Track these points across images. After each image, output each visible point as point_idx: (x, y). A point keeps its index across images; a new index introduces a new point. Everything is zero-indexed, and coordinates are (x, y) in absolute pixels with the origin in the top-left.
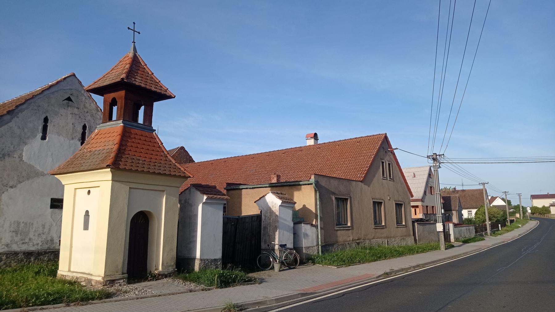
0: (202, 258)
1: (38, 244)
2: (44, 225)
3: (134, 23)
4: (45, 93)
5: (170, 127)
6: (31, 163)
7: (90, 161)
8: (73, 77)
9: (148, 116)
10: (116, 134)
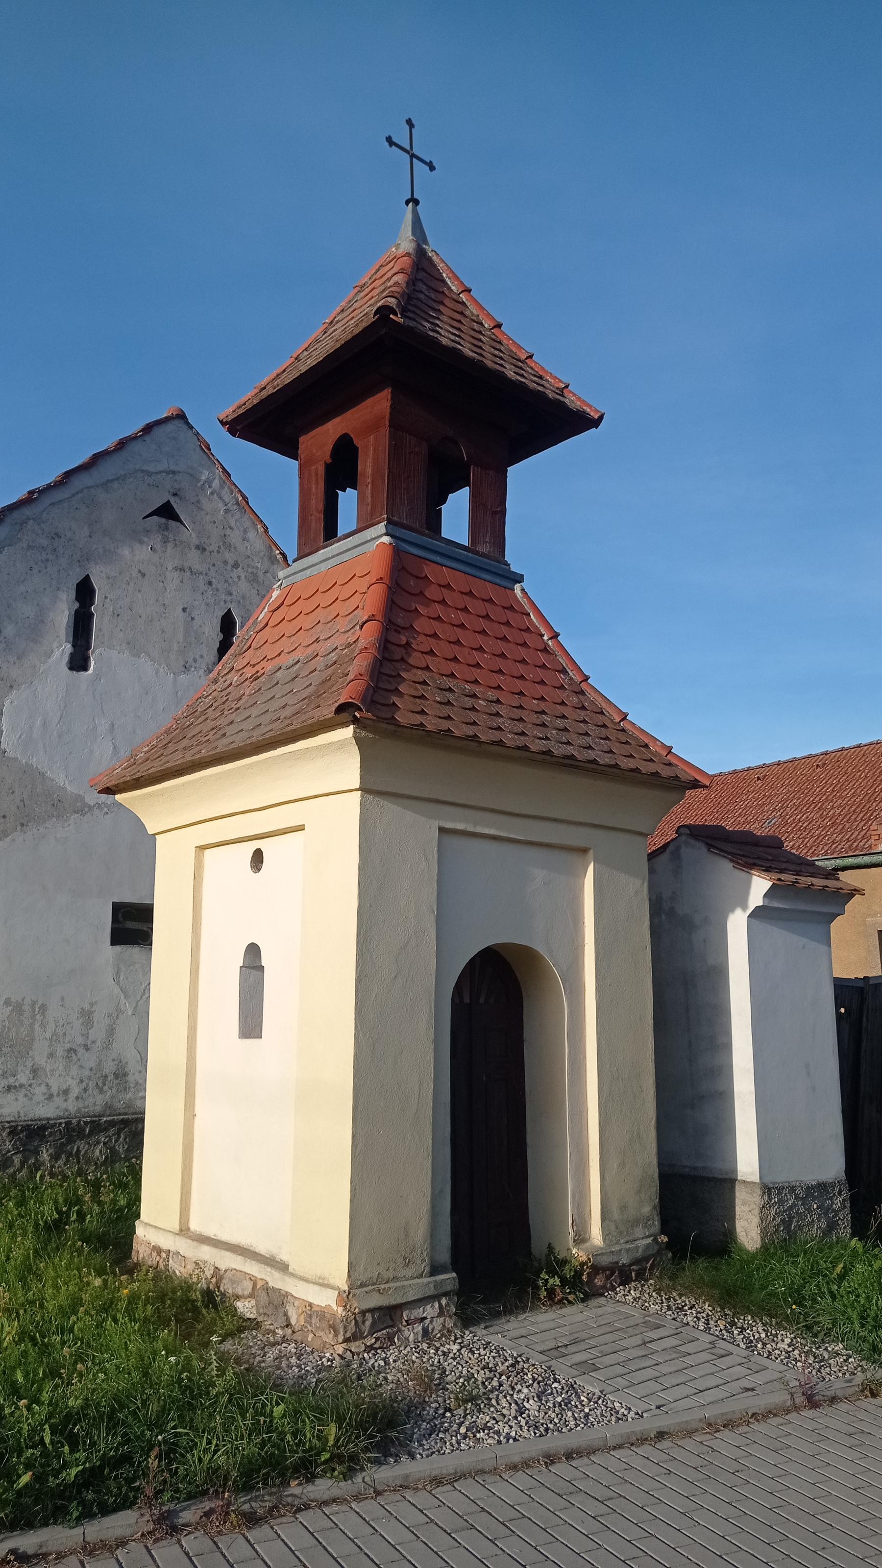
0: (768, 1180)
1: (66, 1092)
2: (90, 1013)
3: (409, 122)
4: (78, 483)
6: (34, 761)
7: (254, 712)
8: (179, 423)
9: (490, 516)
10: (361, 585)
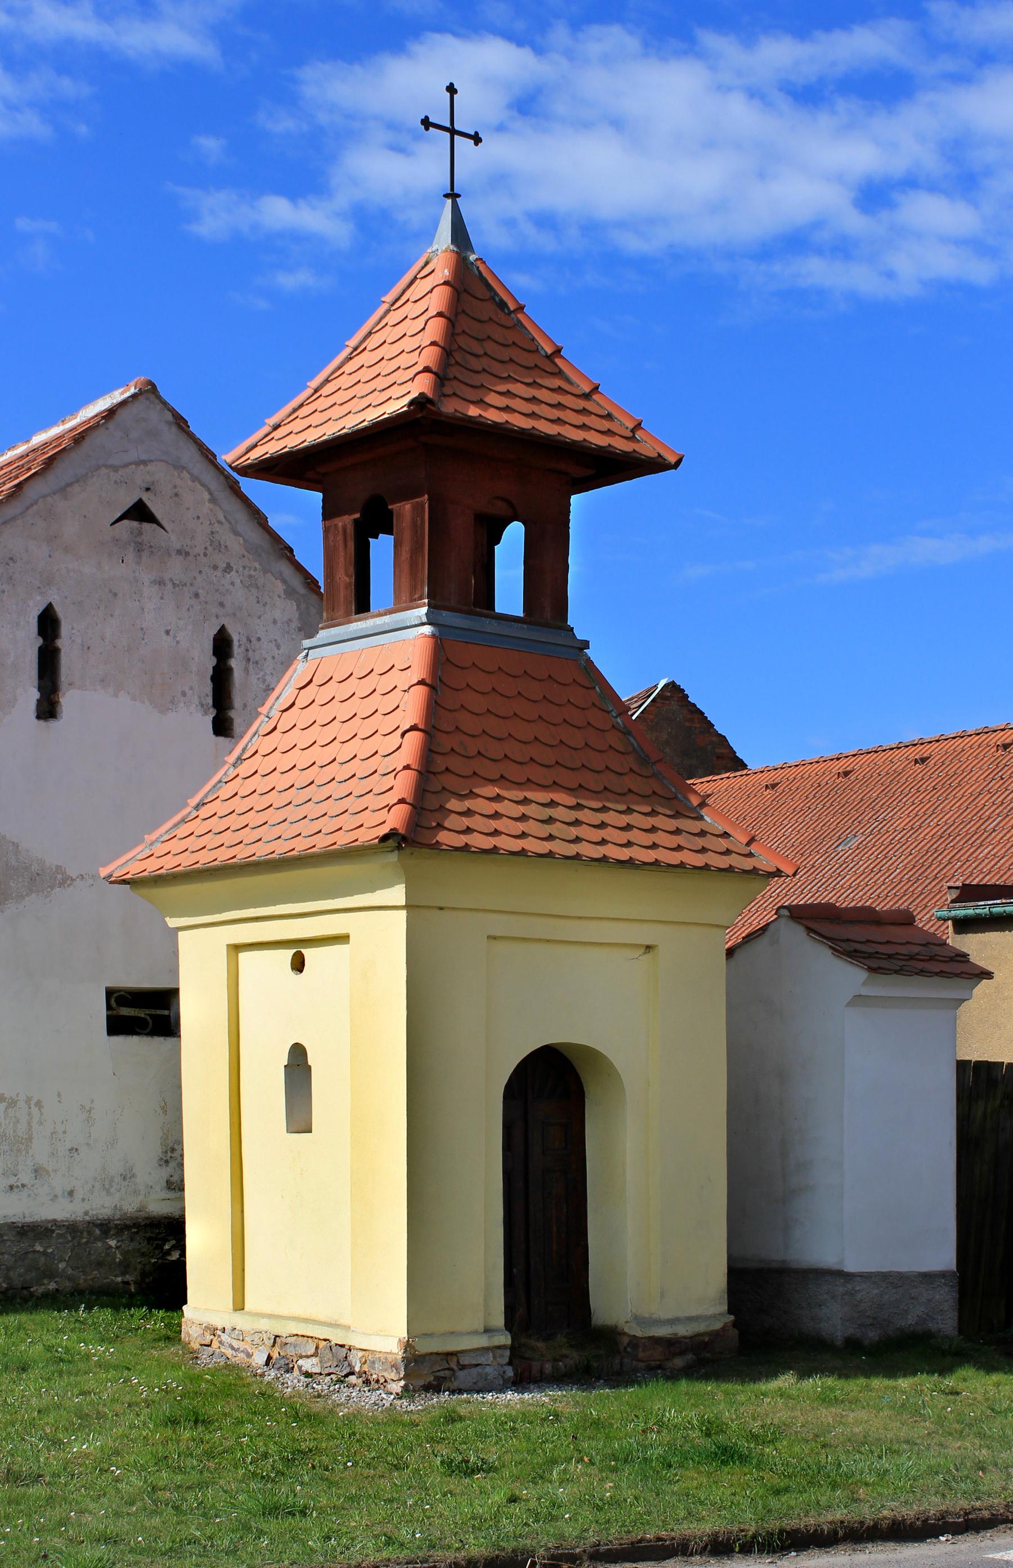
3: (451, 89)
4: (31, 493)
5: (635, 597)
